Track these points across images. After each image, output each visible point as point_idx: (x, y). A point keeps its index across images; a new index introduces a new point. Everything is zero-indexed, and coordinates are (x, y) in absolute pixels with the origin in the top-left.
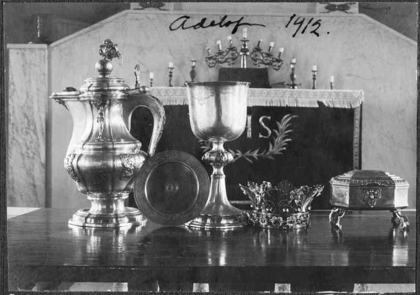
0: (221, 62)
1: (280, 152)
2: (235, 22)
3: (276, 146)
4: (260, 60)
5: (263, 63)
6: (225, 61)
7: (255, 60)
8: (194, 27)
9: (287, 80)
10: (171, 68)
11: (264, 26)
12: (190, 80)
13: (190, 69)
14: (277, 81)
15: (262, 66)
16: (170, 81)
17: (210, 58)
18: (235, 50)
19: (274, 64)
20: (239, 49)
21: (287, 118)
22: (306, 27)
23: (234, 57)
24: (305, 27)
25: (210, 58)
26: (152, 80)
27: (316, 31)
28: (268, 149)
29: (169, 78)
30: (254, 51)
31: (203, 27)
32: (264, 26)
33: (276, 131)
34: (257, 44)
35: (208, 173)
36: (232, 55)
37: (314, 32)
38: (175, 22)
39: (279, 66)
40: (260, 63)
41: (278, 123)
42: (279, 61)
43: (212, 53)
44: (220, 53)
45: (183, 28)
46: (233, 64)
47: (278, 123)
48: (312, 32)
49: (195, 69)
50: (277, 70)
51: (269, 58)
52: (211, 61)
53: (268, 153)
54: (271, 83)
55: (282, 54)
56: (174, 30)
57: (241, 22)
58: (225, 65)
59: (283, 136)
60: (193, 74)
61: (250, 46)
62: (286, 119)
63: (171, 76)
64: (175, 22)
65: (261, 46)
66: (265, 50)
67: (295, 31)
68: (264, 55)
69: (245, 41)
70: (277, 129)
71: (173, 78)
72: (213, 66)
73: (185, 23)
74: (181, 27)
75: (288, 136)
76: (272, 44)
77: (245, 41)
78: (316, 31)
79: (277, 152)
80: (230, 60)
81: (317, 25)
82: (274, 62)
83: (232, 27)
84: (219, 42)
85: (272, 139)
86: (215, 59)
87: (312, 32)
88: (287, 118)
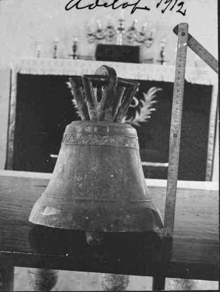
0: (100, 39)
1: (154, 95)
2: (133, 5)
3: (142, 115)
4: (134, 38)
5: (136, 41)
6: (103, 38)
7: (130, 38)
8: (90, 7)
9: (157, 57)
10: (57, 43)
11: (149, 9)
12: (72, 53)
13: (72, 44)
14: (148, 58)
15: (135, 44)
16: (55, 53)
17: (90, 35)
18: (113, 29)
19: (146, 42)
20: (116, 28)
21: (153, 90)
22: (173, 7)
23: (111, 35)
24: (172, 6)
25: (90, 35)
26: (39, 52)
27: (180, 10)
28: (134, 116)
29: (53, 50)
30: (129, 30)
31: (106, 7)
32: (149, 9)
33: (142, 101)
34: (132, 23)
35: (49, 182)
36: (110, 32)
37: (179, 11)
38: (70, 3)
39: (151, 44)
40: (133, 41)
41: (145, 94)
42: (150, 39)
43: (93, 30)
44: (99, 31)
45: (77, 8)
46: (110, 41)
47: (145, 94)
48: (177, 12)
49: (77, 44)
50: (148, 47)
51: (141, 36)
52: (92, 37)
53: (134, 120)
54: (141, 59)
55: (154, 33)
56: (117, 8)
57: (138, 6)
58: (103, 42)
59: (148, 106)
60: (75, 48)
61: (126, 25)
62: (152, 91)
63: (56, 49)
64: (70, 3)
65: (136, 26)
66: (138, 29)
67: (9, 75)
68: (139, 34)
69: (121, 21)
70: (144, 100)
71: (58, 51)
72: (93, 42)
73: (80, 4)
74: (75, 6)
75: (153, 106)
76: (146, 25)
77: (121, 21)
78: (180, 10)
79: (142, 120)
80: (107, 37)
81: (68, 8)
82: (146, 40)
83: (130, 8)
84: (99, 21)
85: (138, 109)
86: (94, 36)
87: (177, 12)
88: (153, 90)
